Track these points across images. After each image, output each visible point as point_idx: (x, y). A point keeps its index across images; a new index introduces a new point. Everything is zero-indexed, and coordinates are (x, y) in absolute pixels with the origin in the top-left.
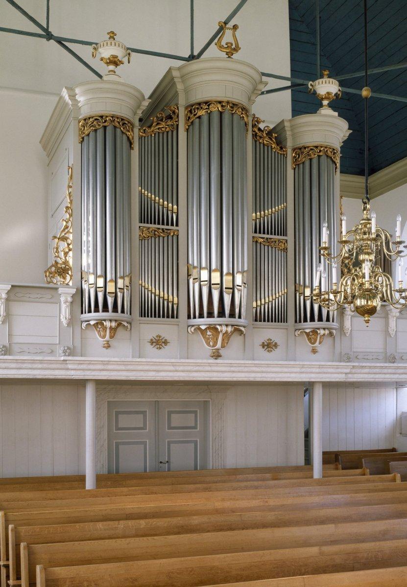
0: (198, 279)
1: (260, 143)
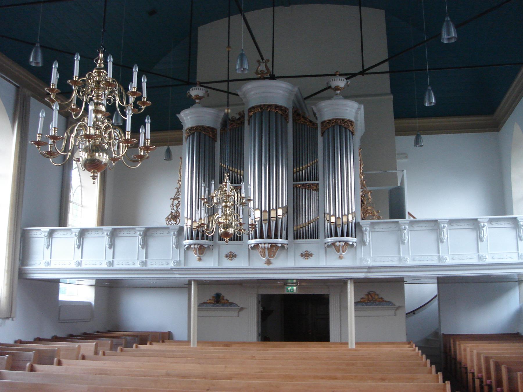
0: (329, 221)
1: (299, 124)
